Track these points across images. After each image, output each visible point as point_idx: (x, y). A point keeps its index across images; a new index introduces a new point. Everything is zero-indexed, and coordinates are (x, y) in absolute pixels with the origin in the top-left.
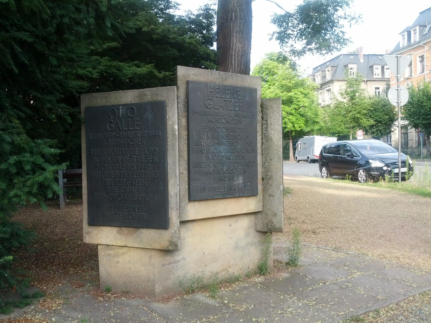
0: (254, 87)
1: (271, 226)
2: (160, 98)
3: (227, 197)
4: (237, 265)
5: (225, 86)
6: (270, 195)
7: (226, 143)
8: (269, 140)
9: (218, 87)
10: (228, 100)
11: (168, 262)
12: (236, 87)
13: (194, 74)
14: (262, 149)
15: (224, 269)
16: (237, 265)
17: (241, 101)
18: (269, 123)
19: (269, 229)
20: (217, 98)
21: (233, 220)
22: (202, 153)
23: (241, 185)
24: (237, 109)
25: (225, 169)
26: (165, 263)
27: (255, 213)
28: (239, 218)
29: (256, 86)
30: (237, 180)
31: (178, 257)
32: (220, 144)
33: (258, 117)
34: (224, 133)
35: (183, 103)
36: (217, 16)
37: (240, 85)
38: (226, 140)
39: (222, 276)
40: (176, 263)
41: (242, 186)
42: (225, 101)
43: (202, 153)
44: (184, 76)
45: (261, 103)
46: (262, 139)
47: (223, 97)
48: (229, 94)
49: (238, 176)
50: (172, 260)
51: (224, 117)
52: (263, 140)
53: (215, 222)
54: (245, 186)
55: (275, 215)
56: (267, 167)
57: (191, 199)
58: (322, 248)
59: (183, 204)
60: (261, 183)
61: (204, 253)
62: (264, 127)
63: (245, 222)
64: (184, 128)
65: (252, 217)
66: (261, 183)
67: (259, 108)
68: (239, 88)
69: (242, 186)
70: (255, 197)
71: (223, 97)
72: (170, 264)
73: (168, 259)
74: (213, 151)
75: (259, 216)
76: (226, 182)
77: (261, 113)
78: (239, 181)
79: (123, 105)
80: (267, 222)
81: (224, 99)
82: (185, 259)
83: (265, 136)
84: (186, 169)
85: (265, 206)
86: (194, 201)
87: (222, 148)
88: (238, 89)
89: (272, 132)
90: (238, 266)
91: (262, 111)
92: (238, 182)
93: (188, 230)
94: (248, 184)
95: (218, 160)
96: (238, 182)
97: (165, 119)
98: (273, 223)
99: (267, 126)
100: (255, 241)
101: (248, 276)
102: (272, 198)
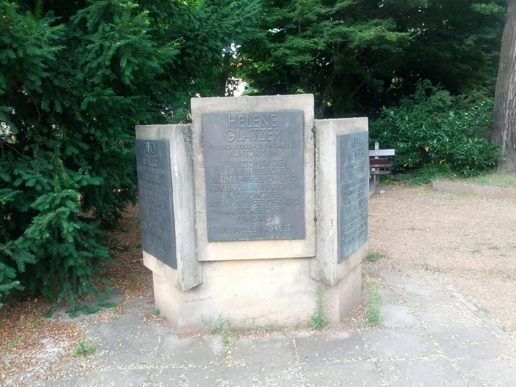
0: (300, 108)
1: (323, 276)
2: (162, 136)
3: (258, 239)
4: (281, 313)
5: (256, 113)
6: (322, 239)
7: (255, 179)
8: (321, 173)
9: (242, 116)
10: (257, 129)
11: (192, 299)
12: (270, 113)
13: (212, 105)
14: (315, 184)
15: (263, 315)
16: (281, 313)
17: (276, 128)
18: (321, 153)
19: (321, 279)
20: (241, 129)
21: (275, 264)
22: (222, 191)
23: (278, 226)
24: (271, 139)
25: (253, 208)
26: (188, 299)
27: (310, 258)
28: (286, 262)
29: (305, 106)
30: (271, 220)
31: (202, 295)
32: (246, 180)
33: (308, 145)
34: (252, 168)
35: (198, 138)
36: (80, 9)
37: (278, 109)
38: (255, 176)
39: (262, 322)
40: (201, 301)
41: (278, 228)
42: (253, 132)
43: (222, 191)
44: (198, 108)
45: (312, 128)
46: (315, 172)
47: (250, 126)
48: (259, 122)
49: (272, 217)
50: (196, 297)
51: (251, 150)
52: (316, 173)
53: (250, 264)
54: (283, 228)
55: (326, 264)
56: (319, 205)
57: (212, 238)
58: (465, 305)
59: (201, 244)
60: (313, 224)
61: (236, 295)
62: (316, 157)
63: (295, 267)
64: (201, 165)
65: (306, 263)
66: (313, 224)
67: (311, 134)
68: (273, 113)
69: (278, 228)
70: (303, 240)
71: (249, 126)
72: (193, 301)
73: (191, 296)
74: (236, 188)
75: (314, 262)
76: (255, 222)
77: (313, 139)
78: (274, 222)
79: (150, 141)
80: (319, 270)
81: (251, 129)
82: (211, 298)
83: (318, 167)
84: (204, 208)
85: (318, 251)
86: (212, 241)
87: (249, 185)
88: (272, 115)
89: (323, 164)
90: (283, 314)
91: (315, 137)
92: (273, 223)
93: (215, 270)
94: (288, 225)
95: (502, 190)
96: (273, 223)
97: (168, 160)
98: (324, 272)
99: (319, 156)
100: (309, 289)
101: (297, 327)
102: (323, 243)
